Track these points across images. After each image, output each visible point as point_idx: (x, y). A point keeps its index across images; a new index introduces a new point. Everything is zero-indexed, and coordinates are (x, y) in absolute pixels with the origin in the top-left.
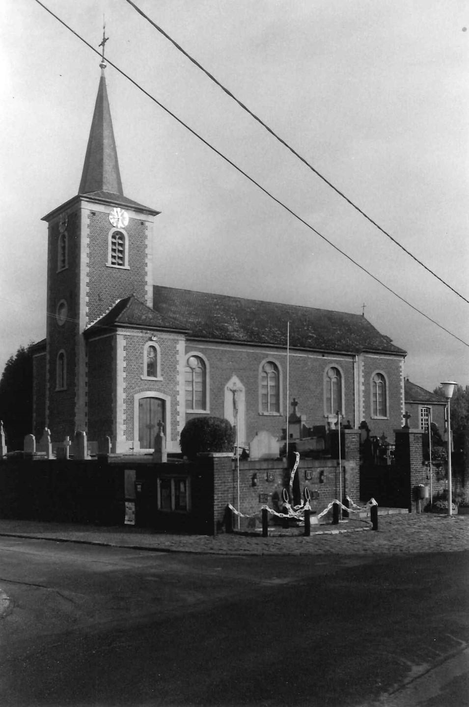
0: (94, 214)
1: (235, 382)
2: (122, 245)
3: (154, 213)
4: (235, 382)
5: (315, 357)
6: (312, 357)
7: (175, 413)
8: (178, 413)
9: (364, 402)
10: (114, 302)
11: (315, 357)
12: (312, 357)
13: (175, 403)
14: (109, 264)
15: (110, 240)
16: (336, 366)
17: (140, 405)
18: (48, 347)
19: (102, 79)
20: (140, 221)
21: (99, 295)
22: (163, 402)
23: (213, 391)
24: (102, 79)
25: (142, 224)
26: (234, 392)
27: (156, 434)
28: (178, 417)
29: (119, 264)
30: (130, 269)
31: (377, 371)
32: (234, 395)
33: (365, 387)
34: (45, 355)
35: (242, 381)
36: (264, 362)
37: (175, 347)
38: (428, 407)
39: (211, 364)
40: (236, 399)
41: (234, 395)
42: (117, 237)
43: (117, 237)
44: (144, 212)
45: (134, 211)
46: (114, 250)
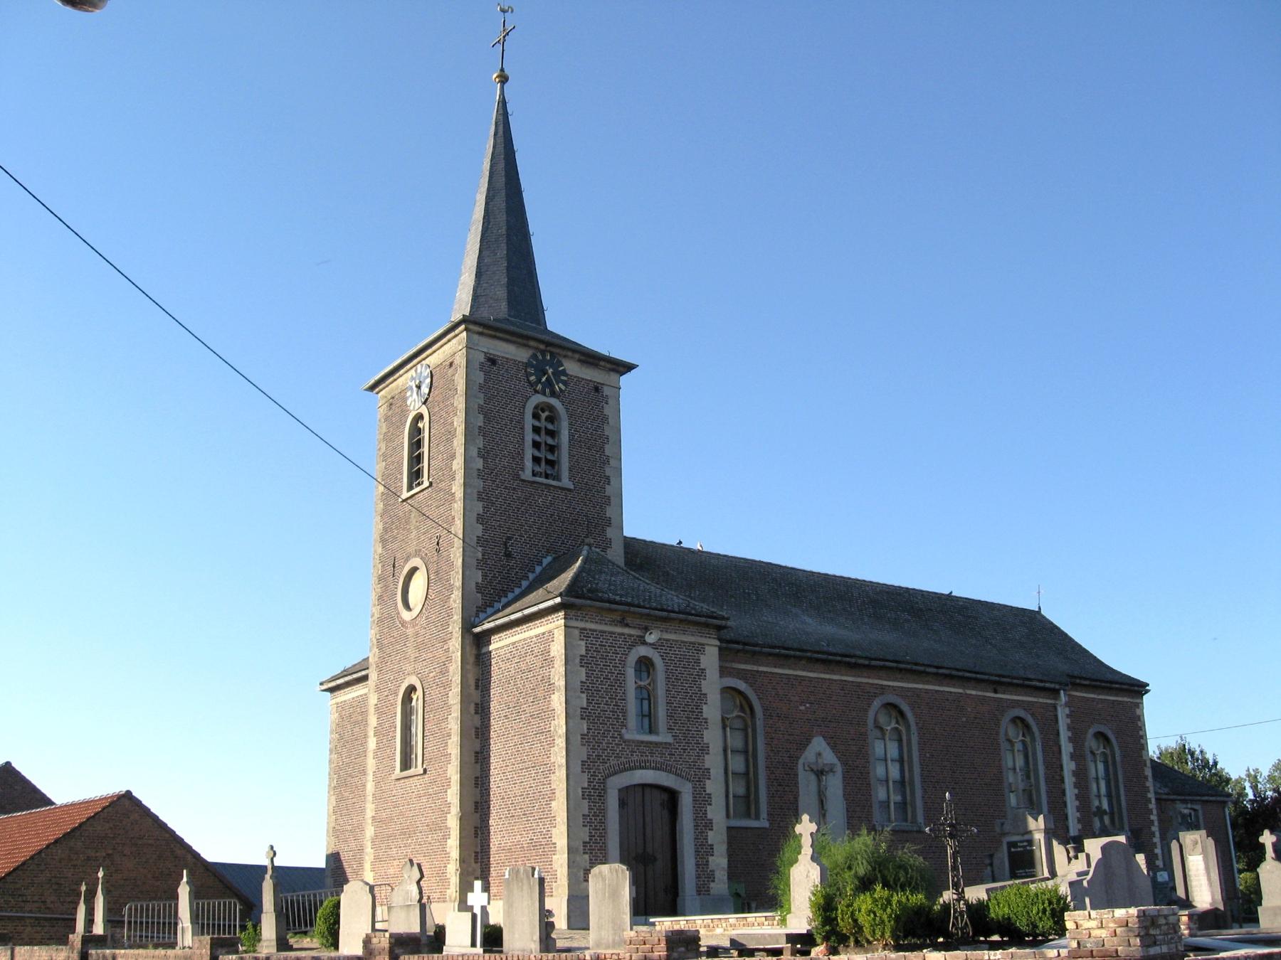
0: (492, 361)
1: (819, 750)
2: (552, 434)
3: (629, 367)
4: (819, 750)
5: (980, 693)
6: (974, 692)
7: (703, 824)
8: (709, 825)
9: (1077, 797)
10: (540, 563)
11: (980, 693)
12: (974, 692)
13: (702, 800)
14: (527, 475)
15: (529, 421)
16: (1022, 714)
17: (623, 804)
18: (373, 676)
19: (503, 103)
20: (591, 384)
21: (505, 544)
22: (672, 797)
23: (773, 773)
24: (503, 103)
25: (597, 389)
26: (820, 773)
27: (1150, 889)
28: (710, 833)
29: (547, 476)
30: (572, 487)
31: (1102, 729)
32: (819, 781)
33: (1077, 765)
34: (364, 698)
35: (834, 748)
36: (877, 703)
37: (698, 662)
38: (1195, 807)
39: (765, 710)
40: (666, 813)
41: (819, 781)
42: (544, 415)
43: (544, 415)
44: (602, 363)
45: (580, 361)
46: (536, 445)
